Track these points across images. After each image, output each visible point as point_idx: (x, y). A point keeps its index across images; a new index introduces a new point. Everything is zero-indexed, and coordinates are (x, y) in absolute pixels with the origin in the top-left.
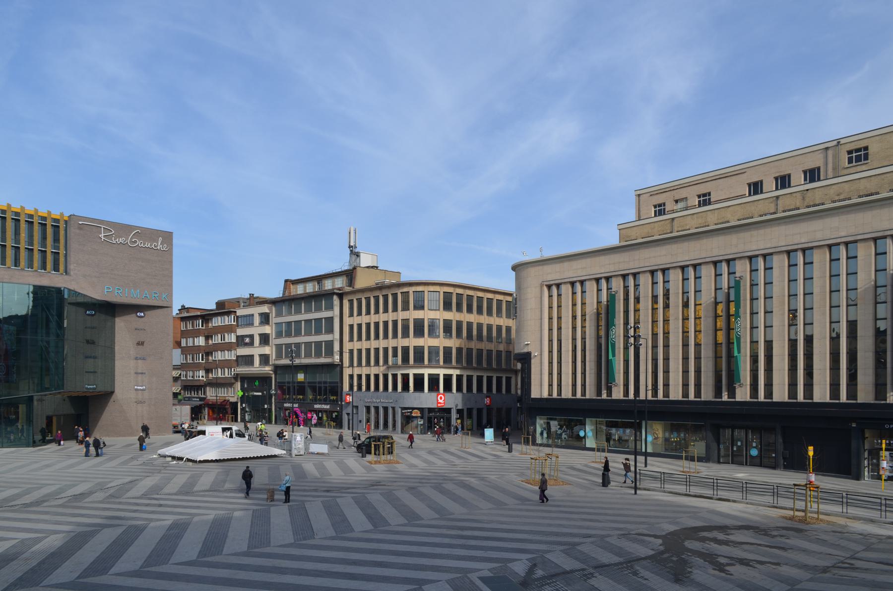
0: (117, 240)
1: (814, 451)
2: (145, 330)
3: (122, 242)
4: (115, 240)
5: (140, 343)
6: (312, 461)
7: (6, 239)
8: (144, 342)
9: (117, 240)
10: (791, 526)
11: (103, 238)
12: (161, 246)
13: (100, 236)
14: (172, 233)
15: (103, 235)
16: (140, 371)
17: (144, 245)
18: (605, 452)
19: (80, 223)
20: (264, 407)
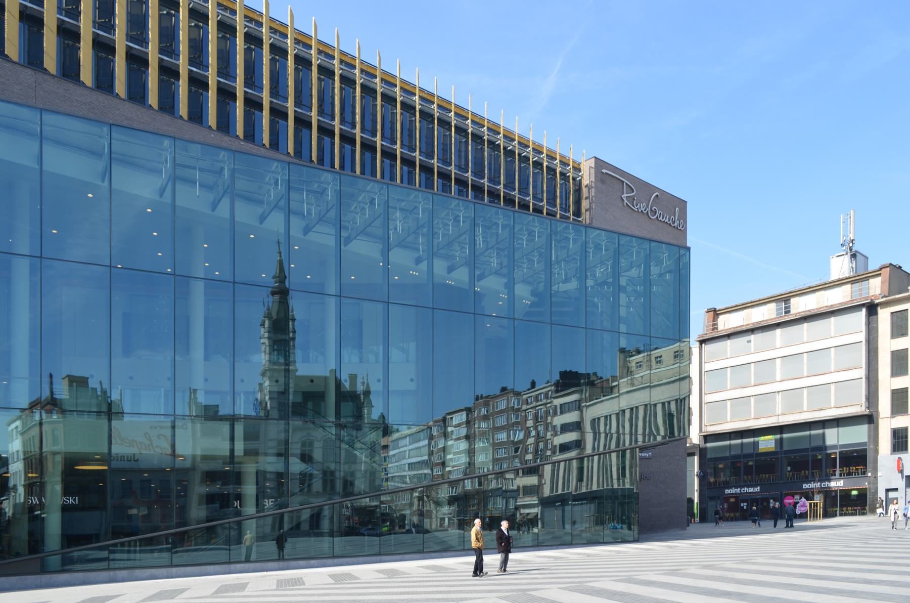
0: (639, 206)
3: (643, 210)
9: (639, 206)
11: (625, 201)
13: (623, 196)
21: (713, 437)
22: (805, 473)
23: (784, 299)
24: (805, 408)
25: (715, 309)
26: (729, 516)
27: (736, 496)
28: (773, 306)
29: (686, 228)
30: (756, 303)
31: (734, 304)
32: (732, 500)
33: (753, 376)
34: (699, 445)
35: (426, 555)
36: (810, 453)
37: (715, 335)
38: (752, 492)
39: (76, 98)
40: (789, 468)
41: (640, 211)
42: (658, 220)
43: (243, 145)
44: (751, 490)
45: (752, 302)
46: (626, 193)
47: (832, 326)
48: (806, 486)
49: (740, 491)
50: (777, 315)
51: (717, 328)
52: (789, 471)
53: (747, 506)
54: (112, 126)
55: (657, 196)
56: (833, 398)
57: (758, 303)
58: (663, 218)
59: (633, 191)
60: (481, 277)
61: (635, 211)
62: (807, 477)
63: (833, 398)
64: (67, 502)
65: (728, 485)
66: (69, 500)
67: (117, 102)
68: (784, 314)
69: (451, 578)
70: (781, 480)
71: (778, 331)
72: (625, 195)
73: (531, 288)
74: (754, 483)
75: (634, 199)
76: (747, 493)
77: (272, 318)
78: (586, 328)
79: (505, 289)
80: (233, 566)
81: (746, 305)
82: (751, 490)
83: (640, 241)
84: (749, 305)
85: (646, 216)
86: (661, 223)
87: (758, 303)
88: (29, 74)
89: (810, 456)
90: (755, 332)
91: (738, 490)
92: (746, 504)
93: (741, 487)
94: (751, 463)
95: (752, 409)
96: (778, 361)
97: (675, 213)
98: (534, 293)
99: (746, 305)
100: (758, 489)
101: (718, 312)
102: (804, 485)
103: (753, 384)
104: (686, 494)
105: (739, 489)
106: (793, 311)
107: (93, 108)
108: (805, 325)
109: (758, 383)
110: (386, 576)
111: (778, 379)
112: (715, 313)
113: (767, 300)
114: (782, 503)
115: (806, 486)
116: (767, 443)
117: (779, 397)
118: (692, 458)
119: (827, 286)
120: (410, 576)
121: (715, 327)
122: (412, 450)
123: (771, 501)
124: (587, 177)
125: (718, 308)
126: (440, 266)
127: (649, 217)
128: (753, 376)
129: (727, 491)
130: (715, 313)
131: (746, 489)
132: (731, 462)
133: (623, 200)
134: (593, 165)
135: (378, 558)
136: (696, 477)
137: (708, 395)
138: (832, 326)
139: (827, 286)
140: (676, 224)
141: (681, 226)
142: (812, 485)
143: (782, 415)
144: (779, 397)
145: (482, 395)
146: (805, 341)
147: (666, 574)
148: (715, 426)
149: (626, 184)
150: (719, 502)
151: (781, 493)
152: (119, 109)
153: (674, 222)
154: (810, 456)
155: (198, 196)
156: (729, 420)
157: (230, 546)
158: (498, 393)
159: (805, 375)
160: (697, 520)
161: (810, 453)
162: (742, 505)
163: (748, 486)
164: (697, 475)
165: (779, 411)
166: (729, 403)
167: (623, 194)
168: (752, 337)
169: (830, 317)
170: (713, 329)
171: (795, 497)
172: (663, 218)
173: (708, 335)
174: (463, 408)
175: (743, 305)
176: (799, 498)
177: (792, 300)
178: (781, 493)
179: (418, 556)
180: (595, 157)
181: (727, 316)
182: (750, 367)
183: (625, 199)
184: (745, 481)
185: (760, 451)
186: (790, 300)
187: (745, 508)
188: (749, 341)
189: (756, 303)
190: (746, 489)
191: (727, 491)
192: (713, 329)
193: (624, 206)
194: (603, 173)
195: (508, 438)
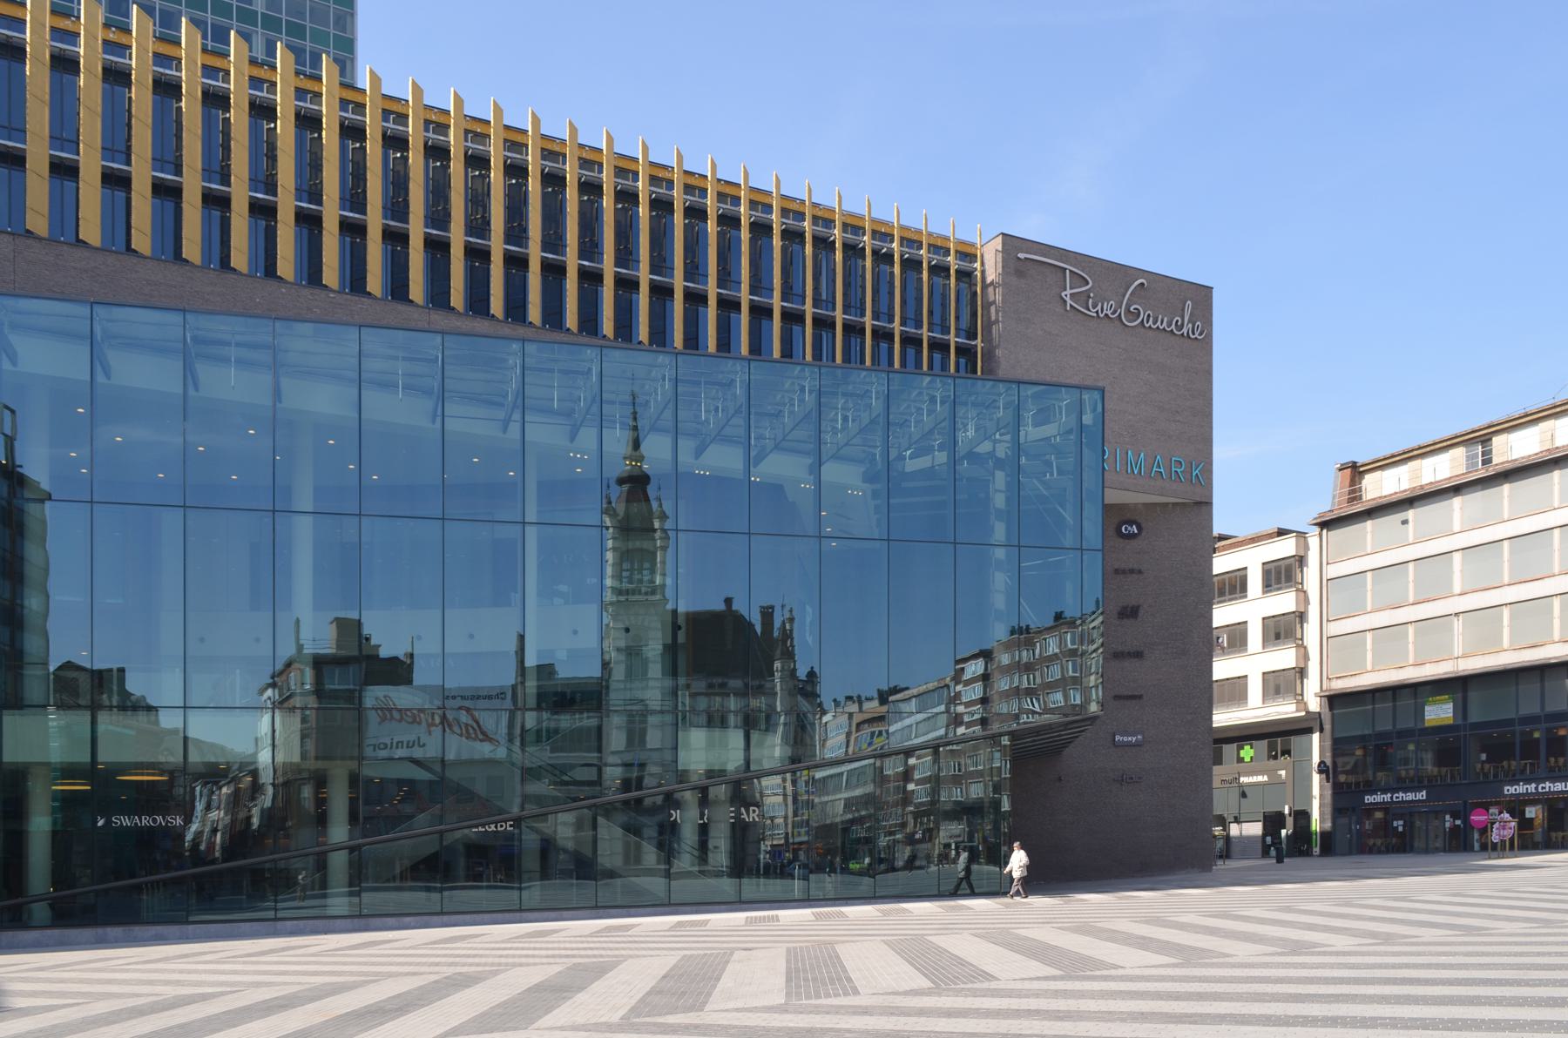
0: (1099, 307)
1: (84, 469)
2: (1140, 572)
3: (1109, 313)
4: (1094, 307)
5: (1129, 613)
6: (865, 1011)
7: (407, 213)
8: (1139, 607)
9: (1099, 307)
10: (378, 1029)
11: (1069, 302)
12: (1190, 325)
13: (1063, 294)
14: (1212, 288)
15: (1068, 292)
16: (897, 715)
17: (1154, 324)
18: (302, 723)
19: (1021, 256)
20: (1487, 756)
21: (1428, 687)
22: (1556, 762)
23: (1481, 438)
24: (1506, 644)
25: (1355, 463)
26: (1374, 844)
27: (1384, 807)
28: (1460, 452)
29: (1209, 336)
30: (1428, 449)
31: (1388, 452)
32: (1379, 815)
33: (1411, 586)
34: (1319, 713)
35: (601, 911)
36: (1518, 728)
37: (1358, 508)
38: (1412, 801)
39: (72, 264)
40: (1484, 757)
41: (1102, 315)
42: (1144, 326)
43: (334, 298)
44: (1410, 796)
45: (1420, 448)
46: (1071, 288)
47: (1556, 488)
48: (1510, 790)
49: (1392, 798)
50: (1467, 468)
51: (1360, 497)
52: (1483, 762)
53: (1404, 826)
54: (94, 305)
55: (1142, 284)
56: (1557, 623)
57: (1432, 448)
58: (1155, 323)
59: (1087, 283)
60: (760, 458)
61: (1093, 317)
62: (1523, 771)
63: (1557, 623)
64: (172, 823)
65: (1372, 788)
66: (175, 820)
67: (135, 261)
68: (1480, 467)
69: (536, 952)
70: (1465, 779)
71: (1457, 502)
72: (1068, 292)
73: (863, 469)
74: (1416, 784)
75: (1089, 297)
76: (1403, 802)
77: (618, 515)
78: (888, 540)
79: (810, 474)
80: (525, 915)
81: (1411, 454)
82: (1410, 796)
83: (1008, 385)
84: (1415, 453)
85: (1119, 324)
86: (1150, 333)
87: (1432, 448)
88: (5, 240)
89: (1518, 735)
90: (1416, 504)
91: (1387, 797)
92: (1401, 822)
93: (1538, 780)
94: (1537, 735)
95: (1411, 647)
96: (1457, 557)
97: (1183, 310)
98: (869, 478)
99: (1411, 454)
100: (1422, 795)
101: (1361, 469)
102: (1366, 797)
103: (1411, 600)
104: (1211, 810)
105: (1389, 795)
106: (1497, 459)
107: (98, 275)
108: (1506, 488)
109: (1421, 598)
110: (929, 938)
111: (1457, 590)
112: (1356, 471)
113: (1449, 443)
114: (1466, 821)
115: (1510, 790)
116: (1440, 712)
117: (1458, 625)
118: (1304, 738)
119: (1558, 409)
120: (973, 932)
121: (1354, 495)
122: (920, 722)
123: (1448, 817)
124: (991, 266)
125: (1360, 460)
126: (686, 446)
127: (1124, 324)
128: (1411, 586)
129: (1369, 799)
130: (1356, 471)
131: (1401, 794)
132: (1376, 746)
133: (1065, 301)
134: (1000, 248)
135: (518, 915)
136: (1316, 778)
137: (1333, 623)
138: (1556, 488)
139: (1558, 409)
140: (1185, 330)
141: (1197, 334)
142: (1521, 789)
143: (1464, 656)
144: (1458, 625)
145: (1028, 626)
146: (1506, 518)
147: (1315, 945)
148: (1346, 680)
149: (1070, 271)
150: (1354, 818)
151: (1465, 803)
152: (136, 272)
153: (1180, 328)
154: (1518, 735)
155: (233, 387)
156: (1369, 668)
157: (520, 883)
158: (1051, 623)
159: (1506, 581)
160: (1316, 850)
161: (1518, 728)
162: (1395, 824)
163: (1406, 790)
164: (1322, 769)
165: (1457, 651)
166: (1369, 635)
167: (1065, 290)
168: (1410, 514)
169: (1552, 471)
170: (1351, 500)
171: (1491, 811)
172: (1155, 323)
173: (1335, 512)
174: (976, 651)
175: (1404, 453)
176: (1497, 811)
177: (1494, 439)
178: (1465, 803)
179: (588, 912)
180: (1003, 234)
181: (1378, 474)
182: (1407, 570)
183: (1068, 299)
184: (1551, 770)
185: (1427, 725)
186: (1491, 439)
187: (1401, 829)
188: (1405, 522)
189: (1428, 449)
190: (1401, 796)
191: (1369, 799)
192: (1351, 500)
193: (1066, 310)
194: (1019, 258)
195: (1066, 701)
